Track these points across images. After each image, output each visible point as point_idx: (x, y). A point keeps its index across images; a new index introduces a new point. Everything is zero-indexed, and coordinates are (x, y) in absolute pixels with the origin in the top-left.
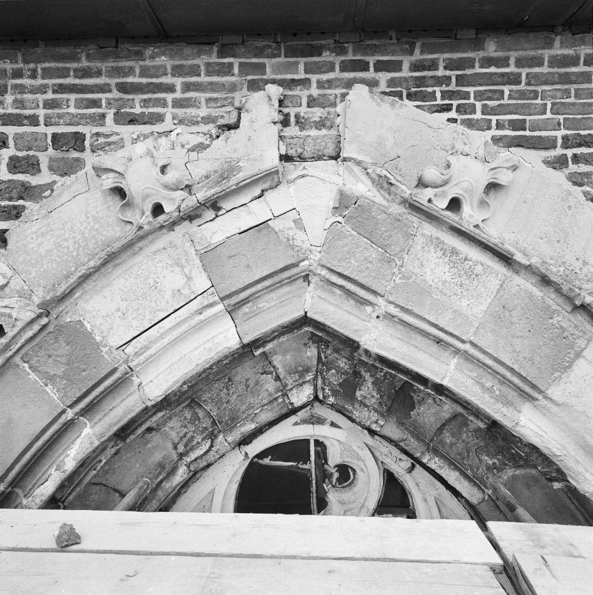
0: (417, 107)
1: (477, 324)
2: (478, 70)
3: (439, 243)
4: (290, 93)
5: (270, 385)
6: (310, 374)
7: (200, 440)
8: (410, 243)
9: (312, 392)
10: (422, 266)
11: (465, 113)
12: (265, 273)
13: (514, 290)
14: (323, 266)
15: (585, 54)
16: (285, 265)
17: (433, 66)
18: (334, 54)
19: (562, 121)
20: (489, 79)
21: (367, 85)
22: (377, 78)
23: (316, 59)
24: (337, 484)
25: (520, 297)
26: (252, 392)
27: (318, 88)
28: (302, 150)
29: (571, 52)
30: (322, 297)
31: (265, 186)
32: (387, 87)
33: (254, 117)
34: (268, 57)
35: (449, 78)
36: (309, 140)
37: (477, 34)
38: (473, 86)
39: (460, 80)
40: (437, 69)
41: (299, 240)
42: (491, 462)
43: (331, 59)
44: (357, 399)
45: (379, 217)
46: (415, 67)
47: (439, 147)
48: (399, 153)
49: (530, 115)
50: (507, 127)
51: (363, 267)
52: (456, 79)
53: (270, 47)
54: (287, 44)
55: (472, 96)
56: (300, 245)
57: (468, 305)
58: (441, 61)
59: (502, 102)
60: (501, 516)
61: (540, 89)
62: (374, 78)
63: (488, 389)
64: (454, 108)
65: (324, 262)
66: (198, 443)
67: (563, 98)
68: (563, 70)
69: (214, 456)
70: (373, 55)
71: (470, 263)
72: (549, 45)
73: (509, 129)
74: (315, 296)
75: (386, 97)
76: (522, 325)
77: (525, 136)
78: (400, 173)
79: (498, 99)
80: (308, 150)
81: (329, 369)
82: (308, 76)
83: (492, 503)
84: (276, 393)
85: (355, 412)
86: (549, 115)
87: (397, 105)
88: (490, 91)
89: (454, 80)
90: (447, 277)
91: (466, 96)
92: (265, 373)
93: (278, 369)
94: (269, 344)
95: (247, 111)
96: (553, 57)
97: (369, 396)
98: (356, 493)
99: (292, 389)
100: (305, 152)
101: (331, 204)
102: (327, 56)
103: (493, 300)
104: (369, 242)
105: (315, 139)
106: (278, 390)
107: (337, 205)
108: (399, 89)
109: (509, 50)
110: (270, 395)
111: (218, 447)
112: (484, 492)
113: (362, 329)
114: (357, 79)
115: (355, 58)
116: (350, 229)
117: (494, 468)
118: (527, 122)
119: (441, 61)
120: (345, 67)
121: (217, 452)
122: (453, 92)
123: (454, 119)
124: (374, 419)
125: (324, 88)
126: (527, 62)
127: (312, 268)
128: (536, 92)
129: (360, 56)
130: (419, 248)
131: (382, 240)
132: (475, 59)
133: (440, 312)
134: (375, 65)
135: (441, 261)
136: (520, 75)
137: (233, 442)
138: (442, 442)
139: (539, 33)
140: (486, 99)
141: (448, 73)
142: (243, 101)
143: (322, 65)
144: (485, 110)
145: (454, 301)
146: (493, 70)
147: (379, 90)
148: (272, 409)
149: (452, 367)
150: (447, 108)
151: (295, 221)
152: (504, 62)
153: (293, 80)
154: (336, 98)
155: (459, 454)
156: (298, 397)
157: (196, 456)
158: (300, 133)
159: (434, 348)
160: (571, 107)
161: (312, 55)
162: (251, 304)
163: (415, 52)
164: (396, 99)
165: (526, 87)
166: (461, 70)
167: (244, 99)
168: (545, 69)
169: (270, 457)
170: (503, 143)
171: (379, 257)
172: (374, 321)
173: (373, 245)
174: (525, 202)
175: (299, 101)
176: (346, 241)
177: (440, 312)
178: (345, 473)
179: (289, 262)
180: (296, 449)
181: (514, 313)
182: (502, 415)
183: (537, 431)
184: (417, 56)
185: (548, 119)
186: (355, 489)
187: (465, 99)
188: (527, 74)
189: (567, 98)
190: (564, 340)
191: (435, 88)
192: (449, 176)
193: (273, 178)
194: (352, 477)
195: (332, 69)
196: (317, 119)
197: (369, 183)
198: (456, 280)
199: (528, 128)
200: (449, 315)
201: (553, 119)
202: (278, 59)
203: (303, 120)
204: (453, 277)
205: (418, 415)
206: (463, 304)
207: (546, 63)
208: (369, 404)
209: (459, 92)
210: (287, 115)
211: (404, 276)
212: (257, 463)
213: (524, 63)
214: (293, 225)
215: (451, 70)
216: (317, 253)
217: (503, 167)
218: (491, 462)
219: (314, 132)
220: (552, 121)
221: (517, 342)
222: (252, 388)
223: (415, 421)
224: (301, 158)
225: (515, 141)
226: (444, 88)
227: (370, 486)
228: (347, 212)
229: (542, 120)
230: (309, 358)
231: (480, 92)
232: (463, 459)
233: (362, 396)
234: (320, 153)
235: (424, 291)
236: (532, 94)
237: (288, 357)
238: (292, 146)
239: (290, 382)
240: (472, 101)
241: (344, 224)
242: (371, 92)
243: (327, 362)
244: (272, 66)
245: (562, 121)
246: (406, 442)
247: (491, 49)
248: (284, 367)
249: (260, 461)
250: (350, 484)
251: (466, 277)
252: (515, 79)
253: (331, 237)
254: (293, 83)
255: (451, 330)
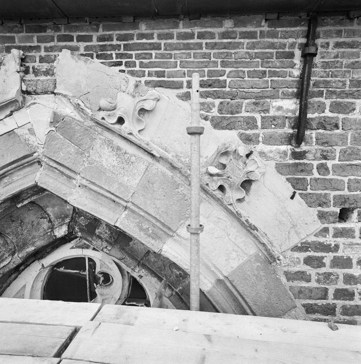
0: (102, 63)
1: (133, 191)
2: (136, 41)
3: (109, 143)
4: (30, 54)
5: (45, 224)
6: (68, 219)
7: (7, 256)
8: (94, 143)
9: (67, 229)
10: (101, 156)
11: (130, 67)
12: (12, 160)
13: (154, 172)
14: (46, 156)
15: (197, 32)
16: (24, 155)
17: (110, 38)
18: (53, 31)
19: (186, 72)
20: (142, 47)
21: (69, 49)
22: (78, 46)
23: (43, 34)
24: (103, 284)
25: (158, 176)
26: (35, 229)
27: (45, 51)
28: (36, 88)
29: (189, 30)
30: (48, 174)
31: (12, 109)
32: (84, 51)
33: (7, 68)
34: (16, 33)
35: (120, 46)
36: (39, 82)
37: (134, 20)
38: (133, 50)
39: (126, 47)
40: (112, 40)
41: (31, 141)
42: (178, 273)
43: (52, 34)
44: (96, 234)
45: (76, 128)
46: (100, 39)
47: (113, 87)
48: (89, 90)
49: (168, 68)
50: (154, 75)
51: (67, 157)
52: (124, 46)
53: (16, 26)
54: (27, 25)
55: (134, 56)
56: (32, 143)
57: (128, 180)
58: (115, 36)
59: (151, 60)
60: (183, 305)
61: (173, 52)
62: (76, 46)
63: (145, 229)
64: (124, 64)
65: (45, 154)
66: (6, 257)
67: (187, 58)
68: (186, 41)
69: (12, 265)
70: (75, 32)
71: (128, 155)
72: (176, 26)
73: (155, 76)
74: (43, 173)
75: (82, 57)
76: (160, 192)
77: (164, 81)
78: (90, 102)
79: (149, 59)
80: (39, 88)
81: (80, 216)
82: (39, 44)
83: (177, 297)
84: (48, 229)
85: (93, 242)
86: (178, 68)
87: (89, 62)
88: (144, 53)
89: (122, 47)
90: (115, 163)
91: (130, 56)
92: (42, 218)
93: (50, 216)
94: (25, 201)
95: (4, 65)
96: (179, 33)
97: (103, 233)
98: (111, 290)
99: (56, 228)
100: (37, 89)
101: (49, 120)
102: (49, 33)
103: (142, 177)
104: (70, 142)
105: (42, 82)
106: (49, 228)
107: (52, 121)
108: (91, 52)
109: (153, 29)
110: (45, 230)
111: (14, 260)
112: (173, 290)
113: (68, 193)
114: (67, 46)
115: (65, 34)
116: (59, 135)
117: (181, 276)
118: (166, 72)
119: (115, 36)
120: (60, 39)
121: (13, 263)
122: (122, 54)
123: (123, 70)
124: (104, 246)
125: (49, 51)
126: (164, 37)
127: (40, 157)
128: (171, 54)
129: (68, 32)
130: (98, 146)
131: (77, 141)
132: (134, 35)
133: (111, 183)
134: (77, 37)
135: (111, 154)
136: (160, 44)
137: (22, 258)
138: (148, 261)
139: (171, 19)
140: (142, 59)
141: (119, 43)
142: (2, 59)
143: (47, 38)
144: (142, 65)
145: (119, 177)
146: (144, 41)
147: (80, 53)
148: (44, 239)
149: (123, 216)
150: (120, 64)
151: (29, 130)
152: (151, 36)
153: (30, 47)
154: (55, 57)
155: (159, 268)
156: (59, 232)
157: (4, 265)
158: (35, 78)
159: (113, 205)
160: (191, 64)
161: (41, 32)
162: (8, 177)
163: (100, 30)
164: (89, 58)
165: (164, 51)
166: (126, 41)
167: (3, 58)
168: (175, 41)
169: (64, 267)
170: (151, 85)
171: (76, 151)
172: (77, 188)
173: (72, 144)
174: (165, 120)
175: (34, 59)
176: (56, 141)
177: (111, 183)
178: (107, 279)
179: (26, 153)
180: (78, 263)
181: (155, 185)
182: (152, 245)
183: (174, 255)
184: (101, 32)
185: (178, 71)
186: (112, 287)
187: (129, 58)
188: (165, 44)
189: (189, 58)
190: (185, 201)
191: (112, 52)
192: (115, 104)
193: (16, 105)
194: (111, 280)
195: (53, 40)
196: (44, 70)
197: (72, 108)
198: (120, 166)
199: (166, 75)
200: (116, 186)
201: (181, 70)
202: (22, 34)
203: (36, 71)
204: (118, 163)
205: (134, 244)
206: (125, 179)
207: (175, 37)
208: (103, 237)
209: (126, 54)
210: (28, 67)
211: (90, 163)
212: (56, 270)
213: (162, 37)
214: (28, 132)
215: (120, 41)
216: (42, 148)
217: (150, 99)
218: (178, 273)
219: (43, 78)
220: (180, 72)
221: (157, 202)
222: (35, 226)
223: (132, 247)
224: (35, 93)
225: (158, 83)
226: (117, 52)
227: (119, 286)
228: (58, 125)
229: (175, 71)
230: (68, 210)
231: (138, 54)
232: (161, 271)
233: (99, 232)
234: (46, 90)
235: (101, 171)
236: (169, 56)
237: (56, 209)
238: (30, 85)
239: (56, 223)
240: (134, 59)
241: (56, 132)
242: (72, 54)
243: (79, 212)
244: (19, 38)
245: (186, 72)
246: (125, 260)
247: (143, 28)
248: (54, 214)
249: (58, 269)
250: (110, 284)
251: (126, 164)
252: (157, 47)
253: (49, 139)
254: (31, 48)
255: (117, 195)
